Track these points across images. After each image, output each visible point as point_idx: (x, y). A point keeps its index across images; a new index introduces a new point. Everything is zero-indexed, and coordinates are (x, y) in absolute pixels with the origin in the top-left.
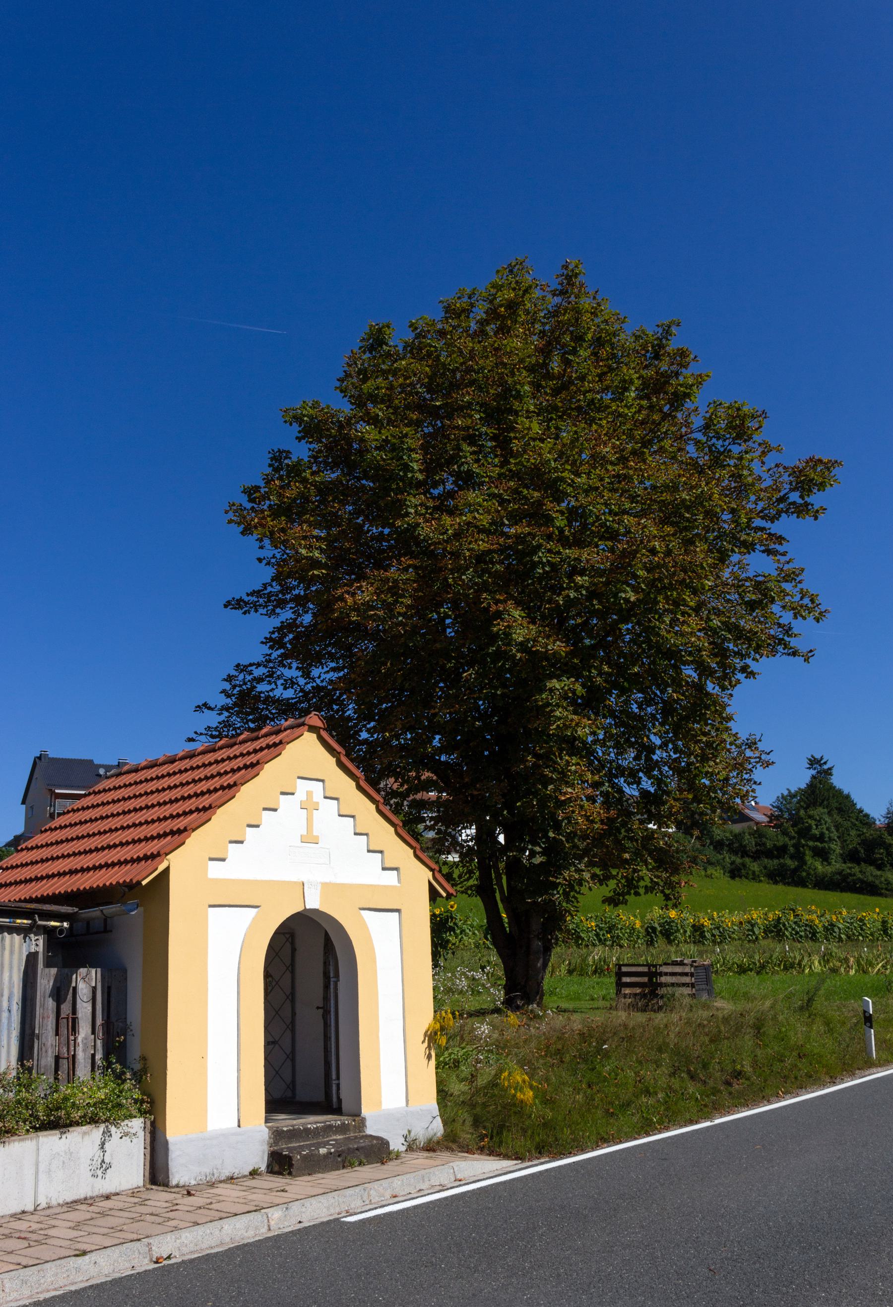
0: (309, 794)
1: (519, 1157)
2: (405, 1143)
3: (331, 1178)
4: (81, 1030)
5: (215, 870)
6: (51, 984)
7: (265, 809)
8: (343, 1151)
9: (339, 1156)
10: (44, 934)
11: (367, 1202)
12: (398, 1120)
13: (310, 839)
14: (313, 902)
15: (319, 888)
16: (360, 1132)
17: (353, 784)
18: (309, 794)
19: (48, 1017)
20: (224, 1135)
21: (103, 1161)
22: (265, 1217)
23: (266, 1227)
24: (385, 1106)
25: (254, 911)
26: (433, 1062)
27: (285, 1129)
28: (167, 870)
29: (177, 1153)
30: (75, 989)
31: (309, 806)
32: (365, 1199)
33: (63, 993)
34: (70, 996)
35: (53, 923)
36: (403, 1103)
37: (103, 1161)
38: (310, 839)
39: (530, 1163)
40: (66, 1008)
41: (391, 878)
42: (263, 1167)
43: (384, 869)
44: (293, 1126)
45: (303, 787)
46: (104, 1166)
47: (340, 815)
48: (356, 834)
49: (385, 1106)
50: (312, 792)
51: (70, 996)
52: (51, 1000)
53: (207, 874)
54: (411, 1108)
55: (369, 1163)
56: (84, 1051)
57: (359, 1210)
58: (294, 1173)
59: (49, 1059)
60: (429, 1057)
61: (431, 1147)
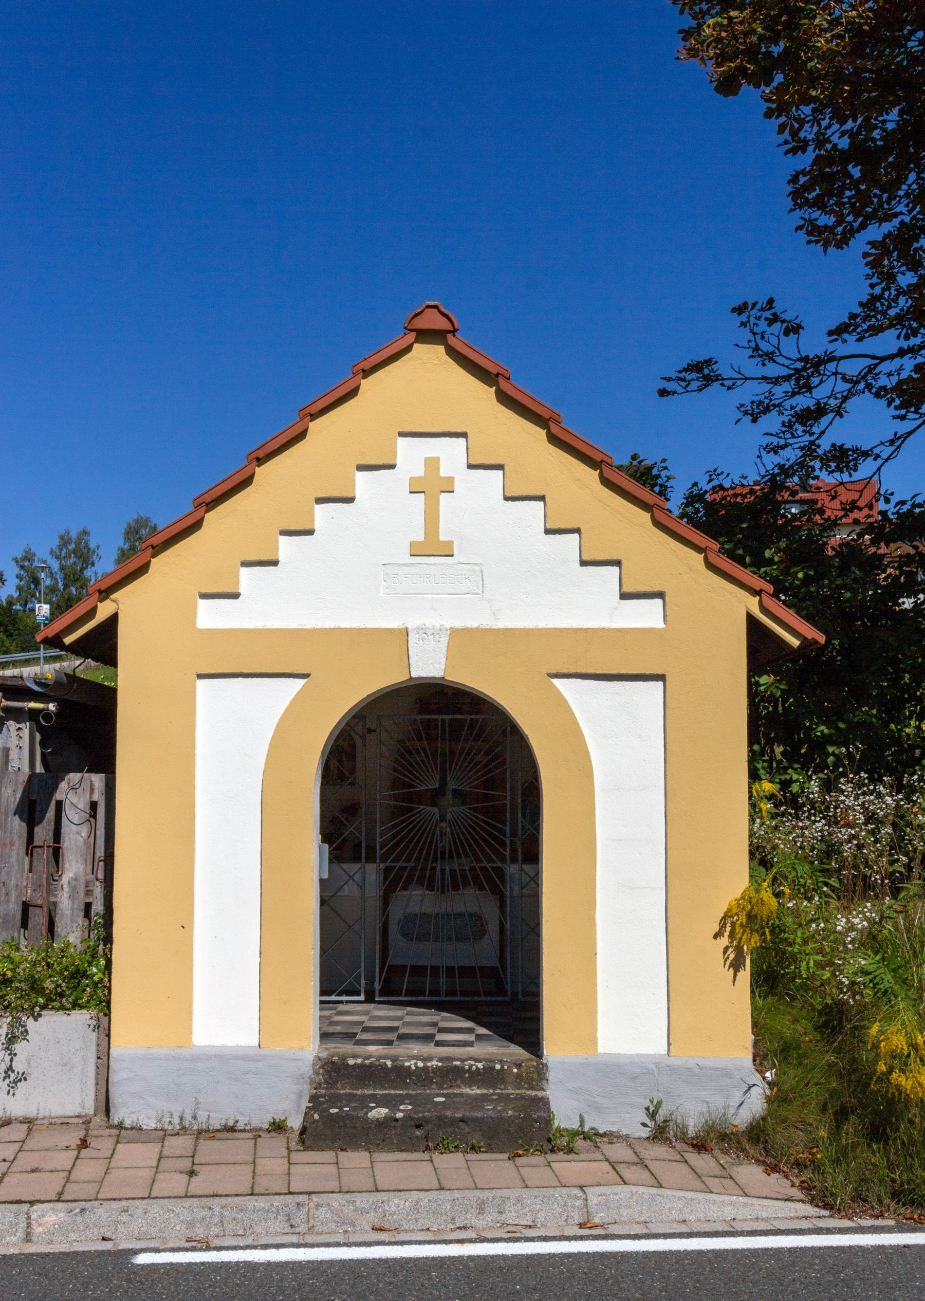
0: (432, 464)
1: (823, 1199)
2: (651, 1124)
3: (392, 1166)
4: (67, 866)
5: (211, 616)
6: (19, 796)
7: (320, 501)
8: (427, 1121)
9: (419, 1126)
10: (30, 720)
11: (302, 1228)
12: (633, 1078)
13: (432, 547)
14: (429, 663)
15: (445, 639)
16: (532, 1088)
17: (543, 433)
18: (432, 464)
19: (12, 844)
20: (224, 1061)
21: (10, 1068)
22: (23, 1218)
23: (21, 1234)
24: (601, 1050)
25: (302, 682)
26: (745, 975)
27: (411, 1064)
28: (113, 620)
29: (124, 1074)
30: (59, 804)
31: (431, 487)
32: (296, 1221)
33: (38, 808)
34: (51, 814)
35: (32, 705)
36: (663, 1050)
37: (10, 1068)
38: (432, 547)
39: (846, 1223)
40: (43, 832)
41: (648, 615)
42: (295, 1123)
43: (624, 596)
44: (450, 1059)
45: (411, 455)
46: (13, 1076)
47: (506, 499)
48: (548, 532)
49: (601, 1050)
50: (438, 459)
51: (51, 814)
52: (17, 818)
53: (195, 623)
54: (672, 1061)
55: (490, 1149)
56: (72, 897)
57: (748, 1227)
58: (308, 1143)
59: (12, 906)
60: (736, 965)
61: (714, 1139)
